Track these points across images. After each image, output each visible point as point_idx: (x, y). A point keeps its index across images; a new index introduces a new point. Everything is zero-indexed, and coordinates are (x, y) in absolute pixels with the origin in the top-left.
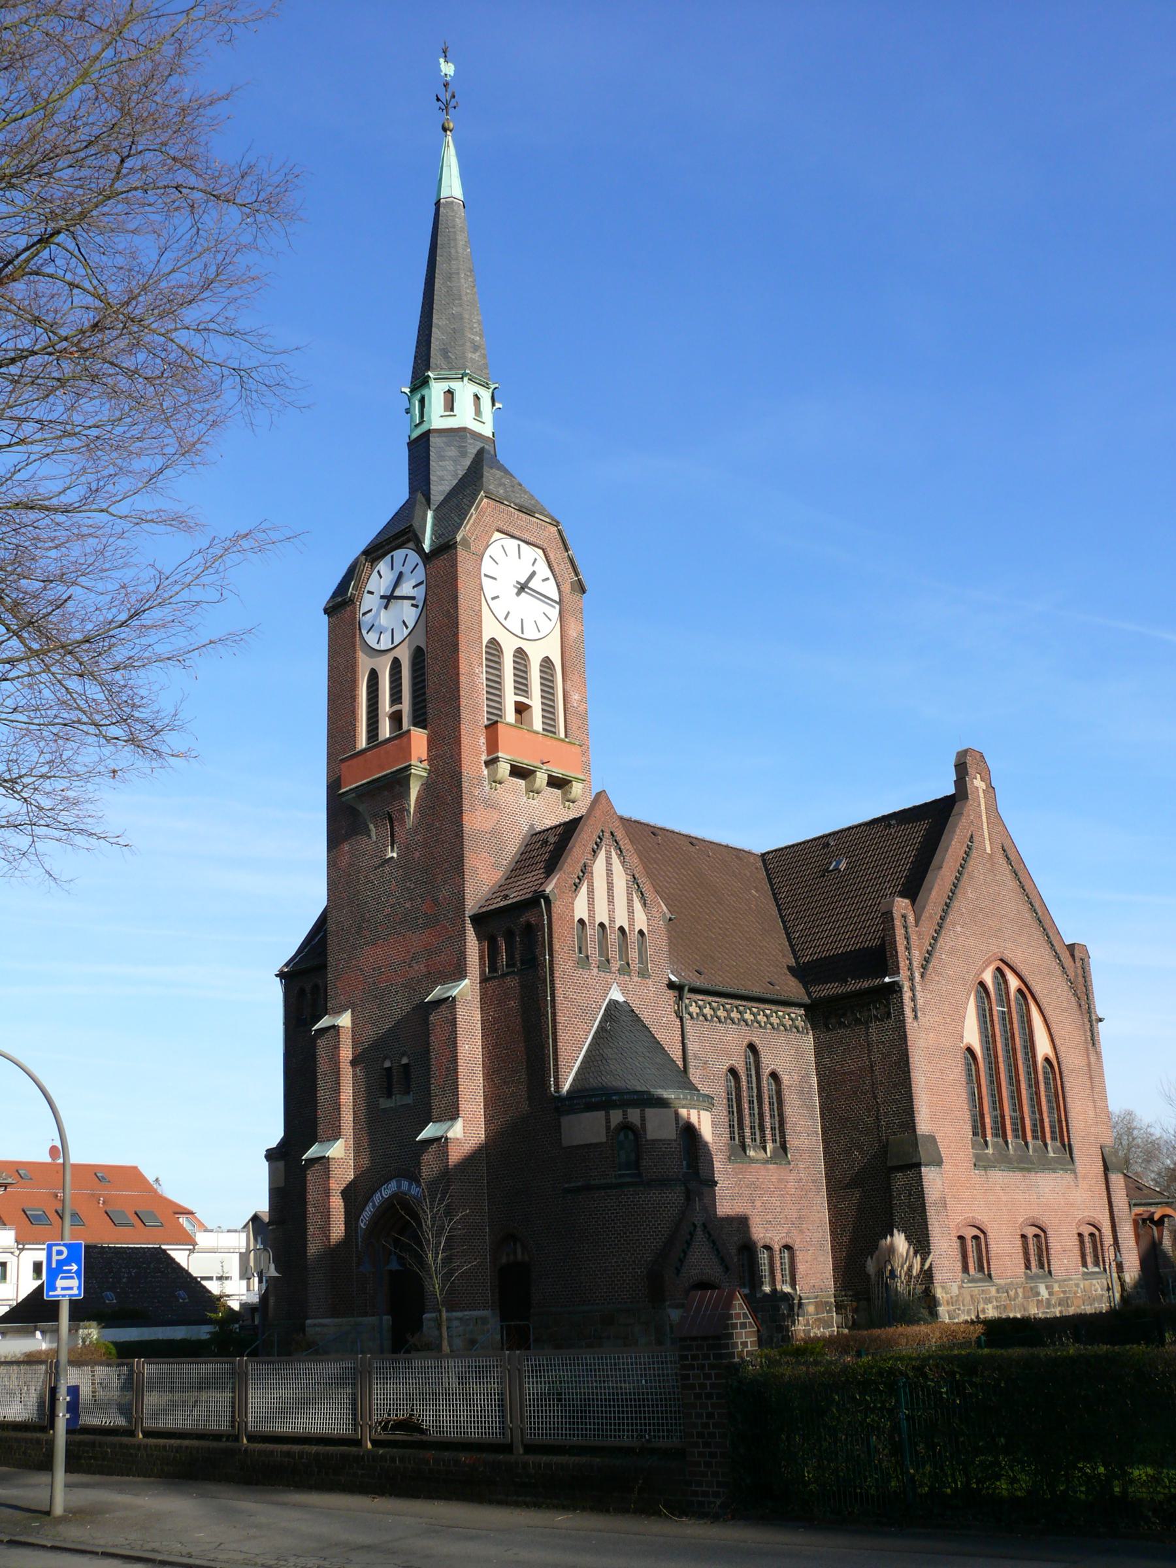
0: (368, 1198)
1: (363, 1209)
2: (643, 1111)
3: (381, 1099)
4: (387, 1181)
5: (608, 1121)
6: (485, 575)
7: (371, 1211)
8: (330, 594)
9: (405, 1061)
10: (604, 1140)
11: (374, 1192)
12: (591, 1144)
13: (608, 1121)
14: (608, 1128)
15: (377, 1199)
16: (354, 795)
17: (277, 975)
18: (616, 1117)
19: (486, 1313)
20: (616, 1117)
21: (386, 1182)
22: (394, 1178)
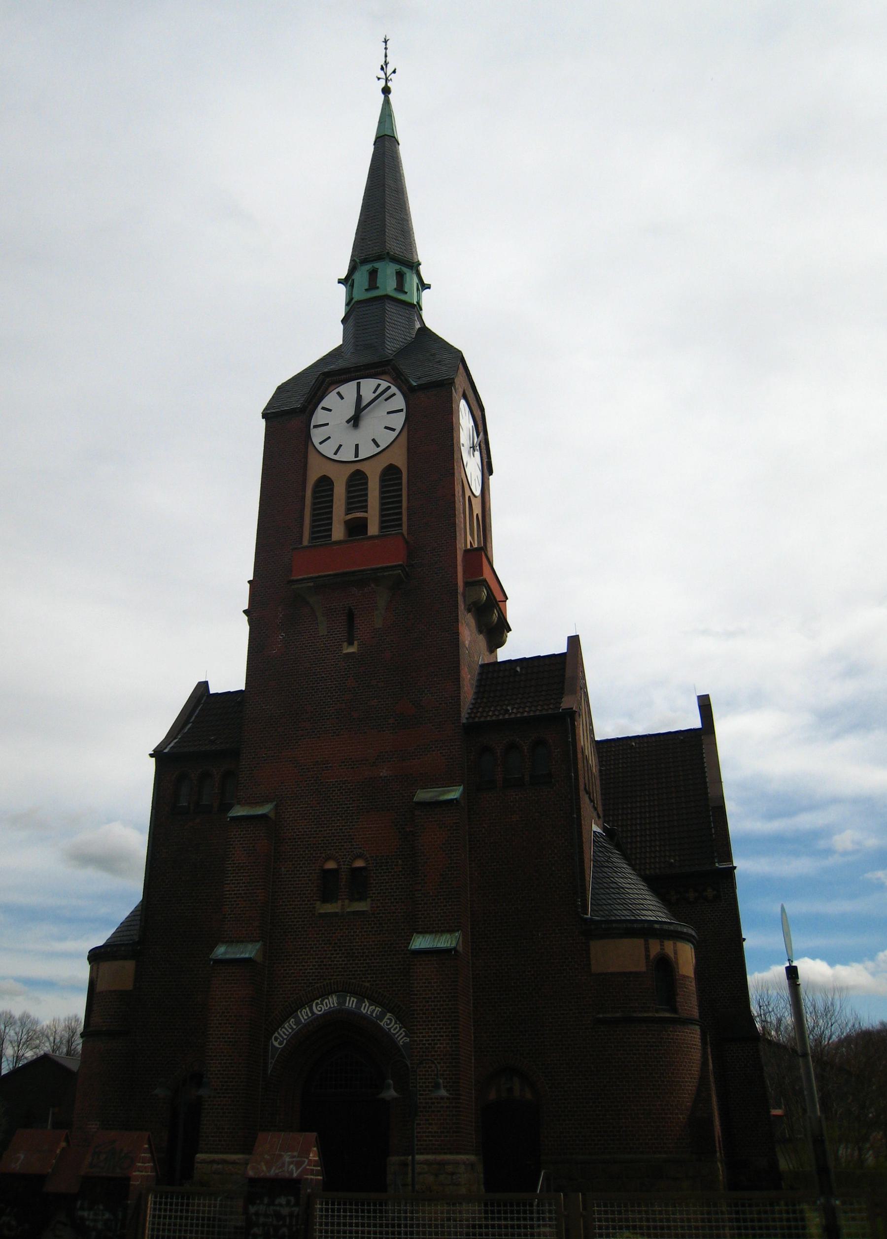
0: (291, 1012)
1: (280, 1024)
2: (675, 943)
3: (319, 902)
4: (324, 995)
5: (647, 950)
6: (336, 453)
7: (292, 1028)
8: (263, 409)
9: (360, 863)
10: (644, 969)
11: (301, 1006)
12: (631, 973)
13: (647, 950)
14: (647, 956)
15: (304, 1015)
16: (311, 584)
17: (151, 755)
18: (655, 948)
19: (472, 1158)
20: (655, 948)
21: (320, 997)
22: (335, 992)
